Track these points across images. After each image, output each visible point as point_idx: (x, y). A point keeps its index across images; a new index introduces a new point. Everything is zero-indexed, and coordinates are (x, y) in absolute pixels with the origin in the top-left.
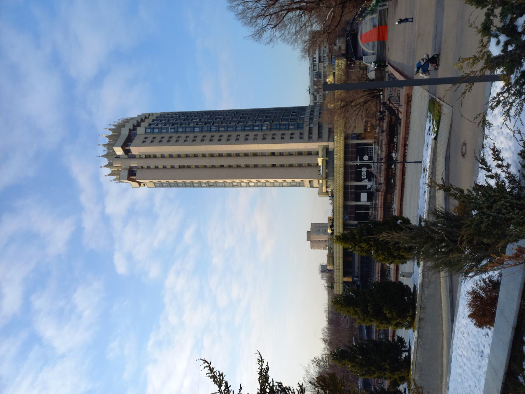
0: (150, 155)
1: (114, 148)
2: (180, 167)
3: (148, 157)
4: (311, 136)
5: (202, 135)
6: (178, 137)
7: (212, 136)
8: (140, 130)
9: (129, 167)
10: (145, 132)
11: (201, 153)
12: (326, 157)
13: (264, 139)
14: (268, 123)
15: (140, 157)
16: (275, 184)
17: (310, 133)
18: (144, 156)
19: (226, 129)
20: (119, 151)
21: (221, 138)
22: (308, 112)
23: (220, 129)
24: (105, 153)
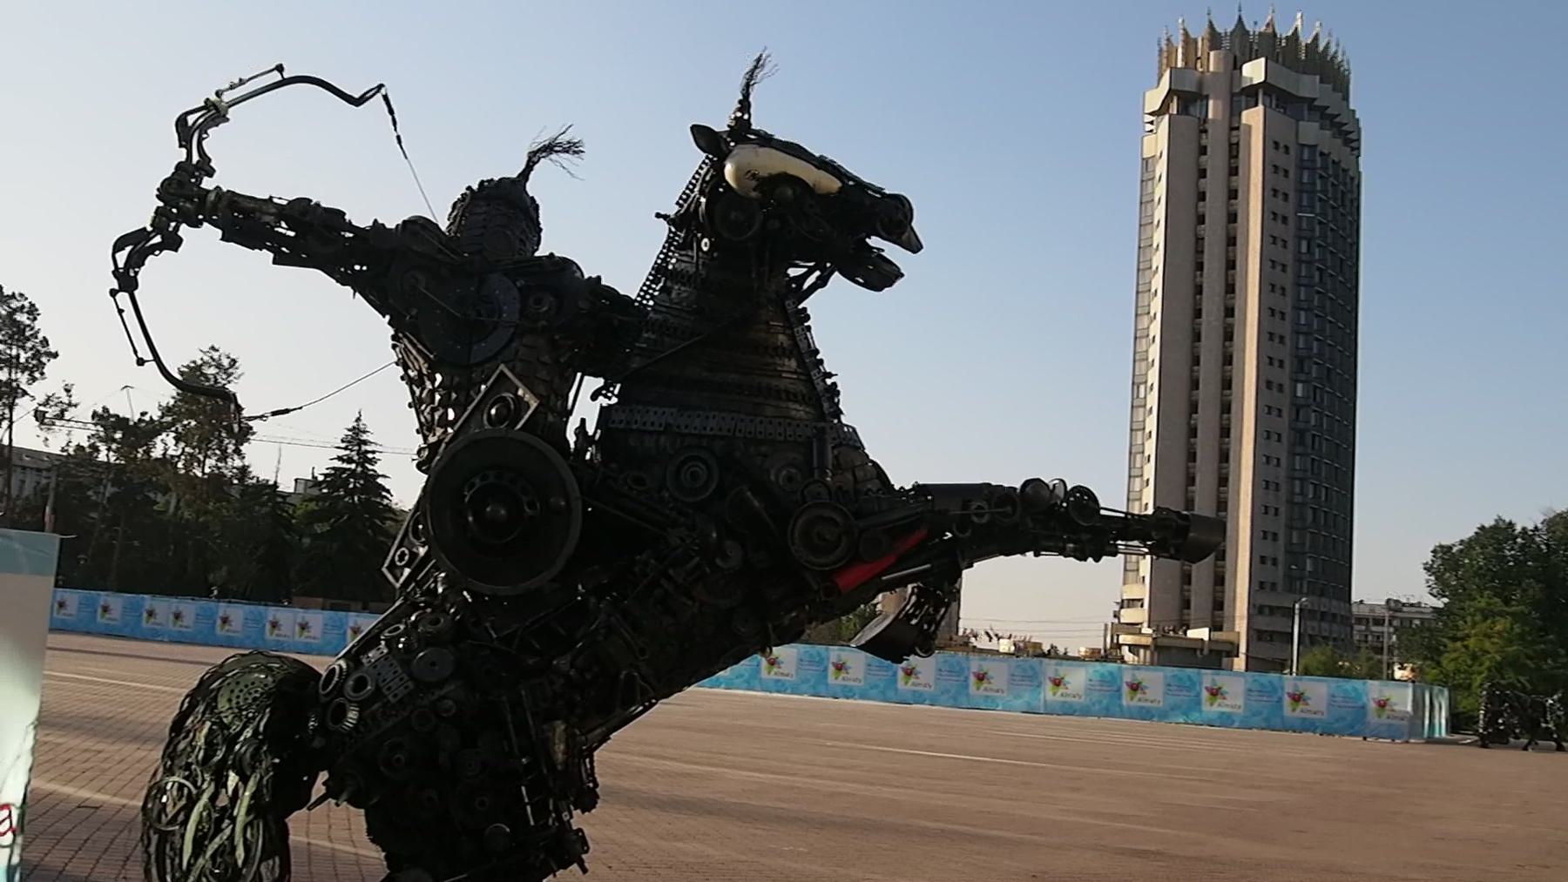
0: (1237, 157)
1: (1263, 60)
2: (1199, 240)
3: (1234, 151)
4: (1267, 611)
8: (1311, 131)
13: (1269, 384)
14: (1317, 279)
15: (1234, 128)
16: (1138, 480)
17: (1273, 610)
18: (1234, 140)
20: (1254, 71)
22: (1335, 606)
24: (1249, 27)
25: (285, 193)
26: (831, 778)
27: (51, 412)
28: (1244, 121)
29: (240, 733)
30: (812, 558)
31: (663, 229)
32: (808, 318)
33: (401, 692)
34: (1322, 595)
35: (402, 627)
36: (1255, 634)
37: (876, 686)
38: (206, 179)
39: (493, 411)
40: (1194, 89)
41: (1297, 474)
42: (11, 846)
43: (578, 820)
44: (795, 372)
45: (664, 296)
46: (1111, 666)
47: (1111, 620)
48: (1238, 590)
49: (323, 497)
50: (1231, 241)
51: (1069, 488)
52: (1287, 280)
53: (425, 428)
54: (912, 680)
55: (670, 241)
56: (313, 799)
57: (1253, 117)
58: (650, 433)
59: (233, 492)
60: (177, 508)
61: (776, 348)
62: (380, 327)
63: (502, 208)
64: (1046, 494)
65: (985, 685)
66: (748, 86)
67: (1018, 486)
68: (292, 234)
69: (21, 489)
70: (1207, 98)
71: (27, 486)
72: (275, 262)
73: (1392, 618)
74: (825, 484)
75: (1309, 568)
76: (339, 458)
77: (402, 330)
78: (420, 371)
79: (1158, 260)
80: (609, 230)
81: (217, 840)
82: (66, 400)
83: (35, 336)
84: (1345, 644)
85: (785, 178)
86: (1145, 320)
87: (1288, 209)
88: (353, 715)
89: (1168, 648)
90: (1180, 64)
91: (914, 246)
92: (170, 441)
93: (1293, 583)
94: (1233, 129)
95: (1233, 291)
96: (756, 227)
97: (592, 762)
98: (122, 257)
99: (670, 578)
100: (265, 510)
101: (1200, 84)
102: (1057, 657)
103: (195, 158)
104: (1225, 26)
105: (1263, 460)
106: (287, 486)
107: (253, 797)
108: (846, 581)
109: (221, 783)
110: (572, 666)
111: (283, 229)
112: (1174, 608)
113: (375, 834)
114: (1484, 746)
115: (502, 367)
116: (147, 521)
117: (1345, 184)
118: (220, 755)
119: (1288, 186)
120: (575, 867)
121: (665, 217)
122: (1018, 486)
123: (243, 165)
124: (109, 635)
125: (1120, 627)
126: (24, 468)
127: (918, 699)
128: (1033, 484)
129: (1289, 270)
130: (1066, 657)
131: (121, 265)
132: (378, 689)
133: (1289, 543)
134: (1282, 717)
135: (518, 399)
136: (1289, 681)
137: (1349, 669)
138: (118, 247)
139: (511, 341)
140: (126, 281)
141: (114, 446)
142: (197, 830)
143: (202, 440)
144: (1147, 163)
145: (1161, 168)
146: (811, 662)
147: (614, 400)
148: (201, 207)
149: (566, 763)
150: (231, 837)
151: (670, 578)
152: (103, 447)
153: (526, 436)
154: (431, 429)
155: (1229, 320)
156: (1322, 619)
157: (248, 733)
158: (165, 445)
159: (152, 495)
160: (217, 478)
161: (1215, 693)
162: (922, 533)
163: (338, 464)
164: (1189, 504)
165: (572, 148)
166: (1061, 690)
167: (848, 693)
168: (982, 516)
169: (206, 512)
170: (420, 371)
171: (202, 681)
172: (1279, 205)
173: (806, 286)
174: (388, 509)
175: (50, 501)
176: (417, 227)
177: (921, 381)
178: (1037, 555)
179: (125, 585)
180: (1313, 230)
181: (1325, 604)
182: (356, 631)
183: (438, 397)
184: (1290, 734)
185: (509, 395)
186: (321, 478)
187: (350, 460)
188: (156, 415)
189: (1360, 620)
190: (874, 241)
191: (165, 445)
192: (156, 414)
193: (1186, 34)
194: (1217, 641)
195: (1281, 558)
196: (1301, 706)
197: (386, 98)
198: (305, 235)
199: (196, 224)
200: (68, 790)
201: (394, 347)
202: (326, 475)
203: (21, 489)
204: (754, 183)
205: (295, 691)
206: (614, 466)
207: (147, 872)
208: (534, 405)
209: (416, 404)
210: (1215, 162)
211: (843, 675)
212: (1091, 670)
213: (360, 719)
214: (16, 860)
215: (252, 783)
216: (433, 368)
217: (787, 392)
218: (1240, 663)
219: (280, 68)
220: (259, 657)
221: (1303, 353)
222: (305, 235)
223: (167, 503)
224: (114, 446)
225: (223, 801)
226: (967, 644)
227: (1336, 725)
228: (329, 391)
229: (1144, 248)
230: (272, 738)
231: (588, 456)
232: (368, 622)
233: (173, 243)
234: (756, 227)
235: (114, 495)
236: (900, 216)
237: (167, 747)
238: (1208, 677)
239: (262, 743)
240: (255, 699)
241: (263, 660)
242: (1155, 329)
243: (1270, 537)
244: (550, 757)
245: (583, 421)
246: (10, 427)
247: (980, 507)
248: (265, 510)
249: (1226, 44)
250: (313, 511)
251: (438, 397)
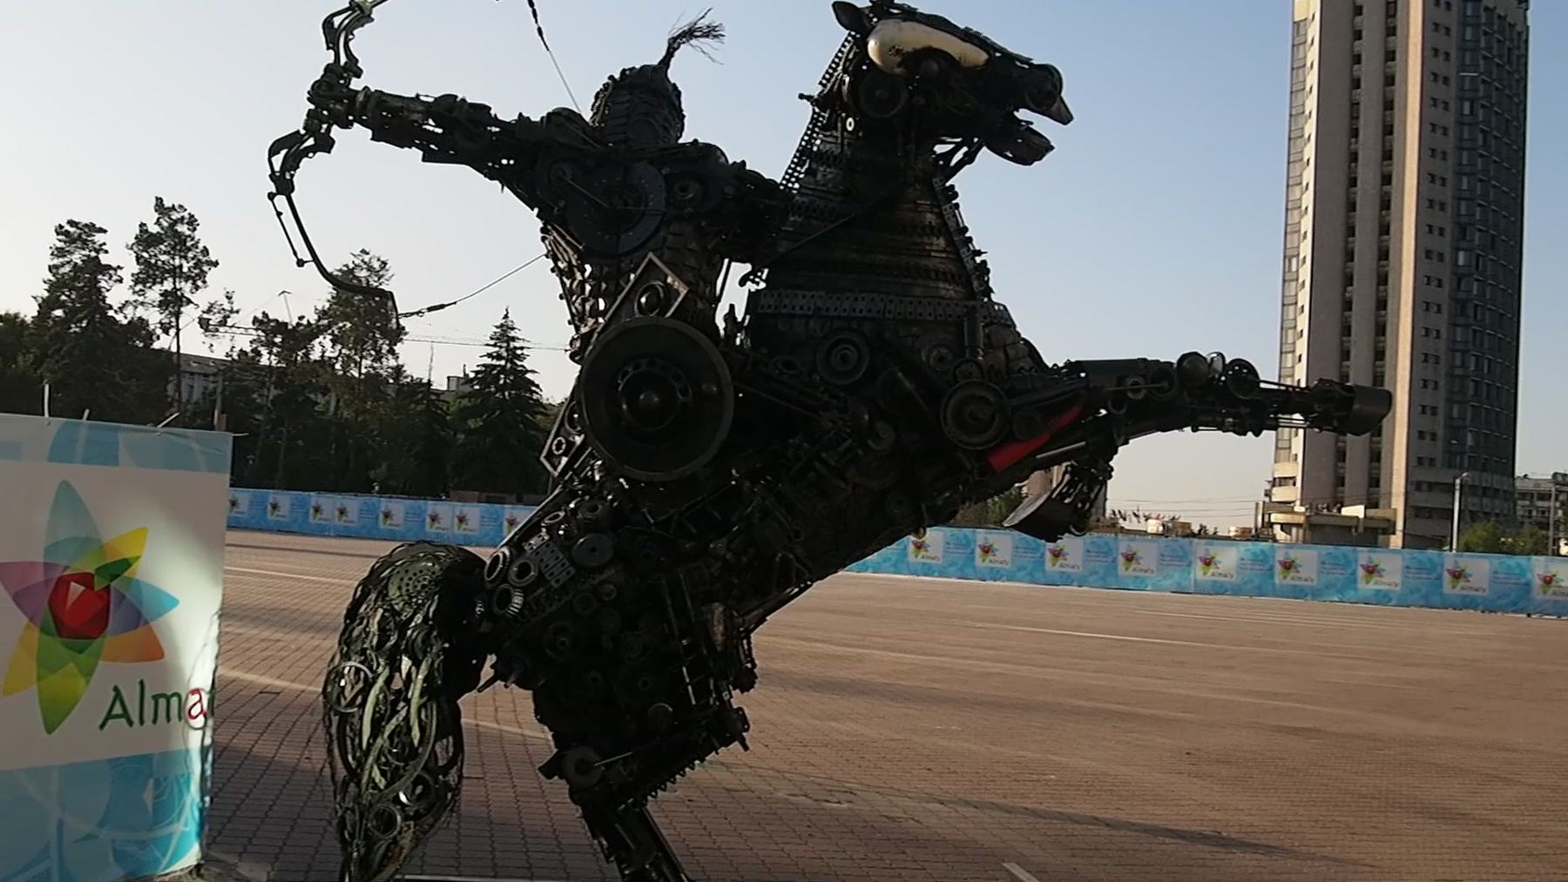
0: (1394, 16)
2: (1355, 105)
4: (1425, 487)
12: (1366, 529)
13: (1428, 254)
14: (1480, 142)
16: (1297, 189)
17: (1431, 486)
19: (1470, 20)
22: (1495, 481)
25: (430, 91)
26: (979, 659)
27: (215, 319)
29: (411, 619)
30: (966, 438)
31: (807, 109)
32: (956, 195)
33: (563, 577)
34: (1484, 470)
35: (562, 514)
36: (1412, 511)
38: (354, 80)
39: (643, 300)
41: (1459, 346)
42: (203, 728)
43: (737, 699)
44: (944, 251)
45: (811, 179)
46: (1263, 545)
47: (1262, 498)
48: (1395, 467)
49: (469, 395)
50: (1389, 105)
51: (1228, 361)
52: (1449, 144)
53: (577, 319)
54: (1060, 561)
55: (814, 121)
56: (482, 683)
58: (801, 317)
59: (390, 391)
60: (337, 407)
61: (924, 228)
62: (530, 220)
63: (644, 96)
64: (1203, 368)
65: (1133, 565)
67: (1174, 361)
68: (439, 131)
69: (190, 394)
71: (194, 390)
72: (424, 160)
73: (1559, 492)
74: (978, 364)
75: (1470, 441)
76: (489, 355)
77: (551, 221)
78: (570, 262)
79: (1311, 128)
80: (755, 113)
81: (394, 721)
82: (227, 306)
83: (195, 246)
84: (1508, 520)
86: (1297, 191)
88: (518, 600)
89: (1322, 526)
91: (1064, 117)
92: (328, 343)
93: (1452, 459)
95: (1390, 158)
96: (902, 102)
97: (749, 643)
98: (278, 161)
99: (823, 462)
100: (420, 408)
102: (1207, 537)
103: (343, 59)
105: (1422, 332)
106: (440, 384)
107: (425, 680)
108: (998, 461)
109: (395, 667)
110: (729, 550)
111: (431, 126)
112: (1328, 483)
113: (543, 715)
115: (651, 255)
116: (315, 420)
117: (1512, 40)
118: (393, 640)
120: (736, 745)
121: (809, 98)
122: (1174, 361)
123: (390, 64)
124: (280, 531)
125: (1270, 506)
126: (192, 374)
127: (1067, 580)
128: (1191, 358)
129: (1451, 133)
130: (1215, 537)
131: (277, 168)
132: (541, 575)
133: (1449, 417)
134: (1441, 594)
135: (668, 287)
136: (1450, 557)
137: (1512, 545)
138: (273, 151)
139: (657, 230)
140: (283, 184)
141: (275, 350)
142: (374, 712)
143: (357, 341)
144: (1298, 27)
145: (1314, 31)
146: (959, 545)
147: (762, 285)
148: (350, 109)
149: (725, 644)
150: (407, 718)
151: (823, 462)
152: (264, 351)
153: (678, 324)
154: (582, 320)
155: (1386, 188)
156: (1484, 495)
157: (419, 619)
158: (324, 346)
159: (312, 396)
160: (373, 379)
161: (1371, 571)
162: (1076, 410)
163: (488, 361)
164: (1345, 377)
165: (711, 32)
166: (1212, 570)
167: (995, 575)
168: (1139, 391)
169: (366, 411)
170: (570, 262)
171: (372, 571)
172: (1439, 65)
173: (953, 162)
174: (538, 403)
175: (219, 404)
176: (562, 118)
177: (1060, 258)
178: (1195, 430)
179: (295, 482)
181: (1488, 480)
182: (512, 523)
183: (588, 288)
184: (1450, 611)
185: (658, 283)
186: (472, 375)
187: (499, 357)
188: (313, 318)
189: (1524, 495)
190: (1023, 114)
191: (324, 346)
192: (312, 318)
194: (1372, 518)
195: (1440, 433)
196: (1462, 583)
198: (451, 131)
199: (346, 125)
200: (250, 677)
201: (543, 239)
202: (477, 373)
203: (190, 394)
204: (898, 59)
205: (460, 578)
206: (764, 351)
207: (330, 751)
208: (683, 291)
209: (567, 295)
211: (990, 557)
212: (1242, 549)
213: (525, 603)
214: (208, 741)
215: (424, 667)
216: (583, 259)
217: (937, 272)
218: (1396, 540)
220: (420, 546)
221: (1463, 220)
222: (451, 131)
223: (326, 403)
224: (275, 350)
225: (397, 684)
227: (1499, 602)
228: (482, 289)
229: (1296, 115)
230: (443, 623)
231: (738, 341)
232: (524, 515)
233: (326, 145)
234: (902, 102)
235: (276, 397)
236: (1049, 87)
237: (343, 634)
238: (1363, 555)
239: (431, 629)
240: (424, 586)
241: (430, 549)
242: (1308, 200)
243: (1428, 412)
244: (711, 644)
245: (732, 307)
246: (177, 334)
247: (1136, 383)
248: (420, 408)
250: (466, 408)
251: (588, 288)
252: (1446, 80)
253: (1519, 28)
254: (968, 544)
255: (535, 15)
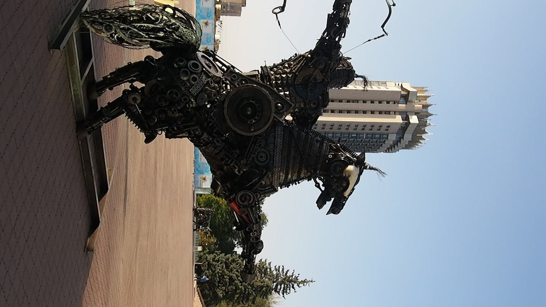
1: (418, 122)
2: (357, 101)
3: (388, 113)
5: (333, 130)
6: (371, 130)
7: (323, 128)
8: (393, 138)
9: (408, 103)
10: (388, 135)
11: (336, 114)
18: (391, 113)
20: (414, 120)
21: (387, 128)
23: (379, 136)
28: (397, 116)
37: (201, 12)
39: (279, 105)
40: (409, 99)
57: (398, 119)
58: (275, 140)
66: (377, 170)
70: (406, 104)
85: (348, 184)
87: (367, 130)
88: (185, 78)
90: (418, 95)
94: (395, 112)
95: (340, 113)
99: (231, 162)
101: (411, 102)
104: (430, 110)
114: (193, 210)
119: (375, 130)
145: (383, 88)
155: (330, 111)
180: (359, 138)
193: (428, 97)
197: (383, 35)
210: (384, 107)
219: (394, 5)
226: (217, 20)
249: (424, 110)
252: (363, 129)
253: (378, 150)
254: (208, 17)
255: (375, 39)
